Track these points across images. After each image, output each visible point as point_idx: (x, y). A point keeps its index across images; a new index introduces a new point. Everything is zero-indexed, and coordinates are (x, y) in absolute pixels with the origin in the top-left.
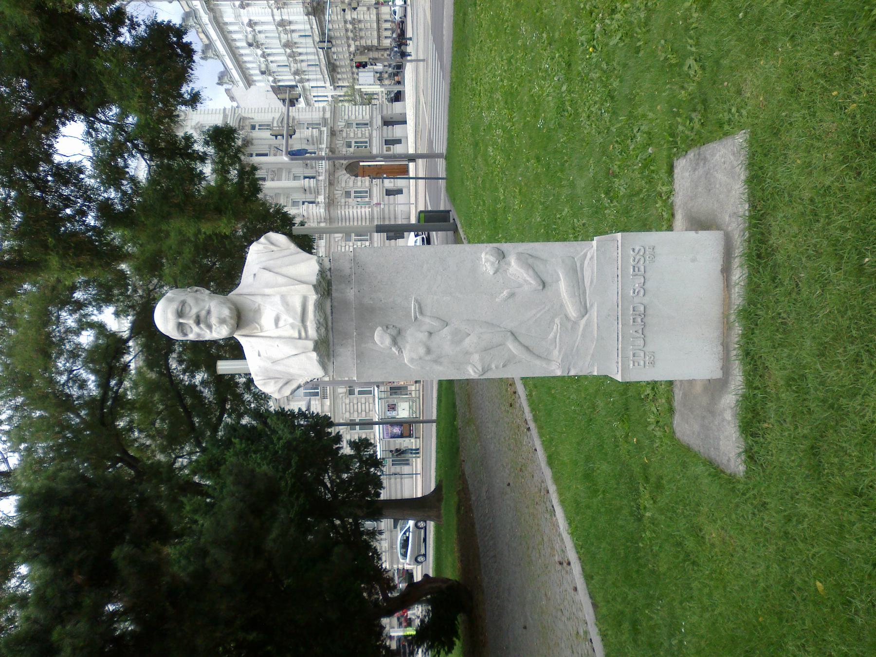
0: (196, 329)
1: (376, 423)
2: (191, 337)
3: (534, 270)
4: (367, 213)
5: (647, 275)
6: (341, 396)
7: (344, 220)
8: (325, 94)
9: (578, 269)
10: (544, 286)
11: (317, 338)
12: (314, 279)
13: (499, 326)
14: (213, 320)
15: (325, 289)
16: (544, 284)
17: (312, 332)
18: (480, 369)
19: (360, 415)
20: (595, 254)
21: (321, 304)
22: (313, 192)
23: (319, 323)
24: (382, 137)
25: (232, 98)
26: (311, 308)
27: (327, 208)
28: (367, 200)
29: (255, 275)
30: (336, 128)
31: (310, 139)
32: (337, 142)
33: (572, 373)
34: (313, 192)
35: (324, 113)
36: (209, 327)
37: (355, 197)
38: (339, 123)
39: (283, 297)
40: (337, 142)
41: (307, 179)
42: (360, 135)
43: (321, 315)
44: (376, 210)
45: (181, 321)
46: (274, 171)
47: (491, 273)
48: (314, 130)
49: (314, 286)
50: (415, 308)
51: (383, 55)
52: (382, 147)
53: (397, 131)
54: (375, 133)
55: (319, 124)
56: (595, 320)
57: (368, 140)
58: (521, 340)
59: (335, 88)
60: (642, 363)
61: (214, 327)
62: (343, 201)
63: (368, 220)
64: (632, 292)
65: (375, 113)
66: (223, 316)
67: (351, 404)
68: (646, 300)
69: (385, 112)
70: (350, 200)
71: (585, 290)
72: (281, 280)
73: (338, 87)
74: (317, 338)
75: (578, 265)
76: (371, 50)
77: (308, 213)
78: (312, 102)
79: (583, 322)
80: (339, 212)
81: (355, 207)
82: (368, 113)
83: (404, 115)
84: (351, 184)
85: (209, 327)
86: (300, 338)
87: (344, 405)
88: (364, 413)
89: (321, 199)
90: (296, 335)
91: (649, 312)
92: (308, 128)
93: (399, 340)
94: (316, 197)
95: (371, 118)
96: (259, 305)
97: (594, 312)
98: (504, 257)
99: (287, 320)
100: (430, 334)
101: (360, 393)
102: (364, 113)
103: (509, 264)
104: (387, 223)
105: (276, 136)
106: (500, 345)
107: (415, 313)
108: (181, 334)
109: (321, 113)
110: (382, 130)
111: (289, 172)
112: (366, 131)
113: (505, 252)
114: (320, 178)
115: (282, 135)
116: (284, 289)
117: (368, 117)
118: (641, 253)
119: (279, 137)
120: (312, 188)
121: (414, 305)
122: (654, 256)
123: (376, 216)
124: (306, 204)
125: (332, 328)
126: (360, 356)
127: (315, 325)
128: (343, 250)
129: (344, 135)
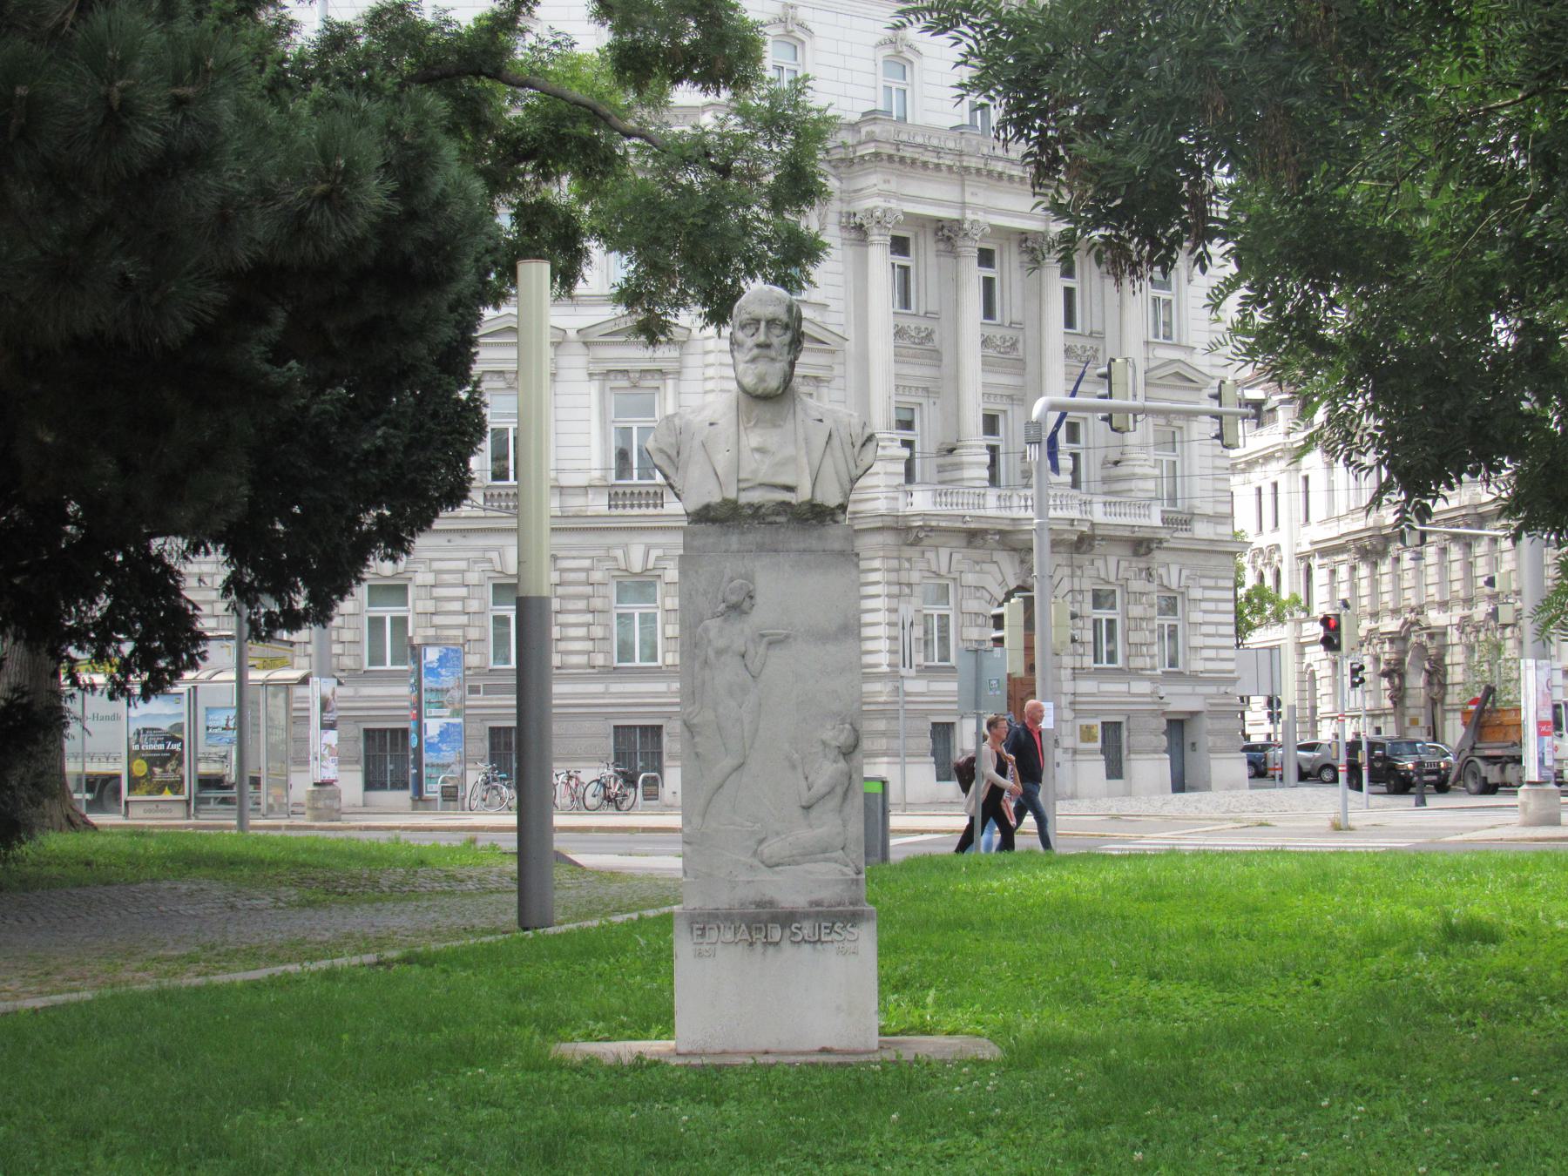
9: (827, 855)
12: (819, 500)
13: (751, 747)
17: (745, 498)
27: (889, 522)
28: (919, 659)
29: (821, 421)
30: (1159, 556)
32: (1112, 561)
38: (1174, 570)
39: (793, 460)
40: (1112, 561)
41: (987, 459)
45: (763, 324)
46: (1014, 346)
50: (777, 634)
51: (1414, 722)
53: (1151, 768)
54: (1142, 687)
57: (1120, 663)
59: (1304, 557)
61: (753, 367)
65: (1212, 690)
66: (768, 379)
72: (817, 455)
73: (1309, 569)
76: (1429, 683)
79: (756, 862)
80: (877, 564)
81: (894, 617)
82: (1210, 666)
83: (1204, 786)
84: (972, 605)
86: (739, 481)
89: (922, 501)
90: (742, 476)
92: (1158, 463)
95: (1195, 678)
96: (780, 426)
107: (772, 635)
109: (1208, 509)
115: (1110, 395)
116: (804, 460)
117: (1198, 665)
120: (956, 475)
124: (906, 453)
129: (1137, 585)
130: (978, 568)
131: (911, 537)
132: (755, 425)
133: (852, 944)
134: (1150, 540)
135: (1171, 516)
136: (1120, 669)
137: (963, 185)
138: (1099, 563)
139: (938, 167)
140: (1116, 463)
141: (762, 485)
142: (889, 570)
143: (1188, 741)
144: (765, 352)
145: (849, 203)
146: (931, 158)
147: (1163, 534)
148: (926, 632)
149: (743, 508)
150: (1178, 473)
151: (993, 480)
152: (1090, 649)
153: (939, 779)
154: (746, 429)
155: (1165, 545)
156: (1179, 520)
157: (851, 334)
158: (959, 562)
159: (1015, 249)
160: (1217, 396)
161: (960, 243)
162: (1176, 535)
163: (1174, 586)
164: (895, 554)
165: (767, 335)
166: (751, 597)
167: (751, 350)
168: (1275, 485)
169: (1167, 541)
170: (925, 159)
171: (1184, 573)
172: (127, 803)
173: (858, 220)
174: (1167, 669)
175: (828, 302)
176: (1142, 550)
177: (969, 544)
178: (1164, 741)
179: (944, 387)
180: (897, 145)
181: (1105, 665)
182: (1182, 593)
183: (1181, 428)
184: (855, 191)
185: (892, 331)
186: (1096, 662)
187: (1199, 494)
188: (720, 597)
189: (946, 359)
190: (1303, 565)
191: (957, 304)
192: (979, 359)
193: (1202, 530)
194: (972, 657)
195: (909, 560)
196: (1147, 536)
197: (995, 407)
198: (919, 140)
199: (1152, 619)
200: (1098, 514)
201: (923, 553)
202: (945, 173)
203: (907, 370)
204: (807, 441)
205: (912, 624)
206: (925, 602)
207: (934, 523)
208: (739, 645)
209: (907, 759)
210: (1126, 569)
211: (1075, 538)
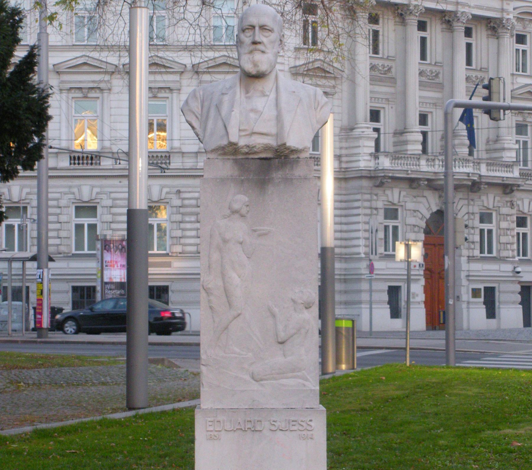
3: (295, 334)
4: (355, 250)
9: (295, 374)
10: (282, 343)
15: (282, 152)
20: (308, 389)
21: (268, 149)
22: (399, 148)
23: (253, 147)
24: (498, 282)
34: (399, 148)
37: (386, 228)
38: (526, 202)
42: (503, 239)
43: (259, 149)
44: (363, 266)
45: (257, 28)
46: (437, 75)
47: (293, 298)
48: (514, 154)
50: (263, 230)
52: (482, 281)
54: (508, 267)
57: (494, 254)
58: (233, 322)
60: (211, 428)
61: (251, 57)
62: (380, 204)
63: (344, 251)
64: (275, 419)
70: (381, 217)
75: (299, 374)
77: (359, 138)
79: (247, 377)
84: (411, 220)
86: (240, 130)
89: (385, 163)
92: (517, 142)
93: (237, 216)
94: (387, 154)
97: (255, 386)
98: (306, 308)
100: (241, 243)
107: (260, 230)
110: (513, 282)
111: (435, 105)
112: (510, 252)
113: (311, 309)
114: (423, 162)
118: (309, 428)
122: (304, 438)
123: (352, 265)
125: (247, 158)
126: (223, 181)
127: (251, 144)
129: (505, 210)
130: (415, 200)
131: (378, 183)
149: (242, 148)
152: (478, 246)
155: (521, 188)
158: (404, 196)
161: (407, 18)
162: (527, 182)
174: (521, 257)
176: (508, 191)
177: (411, 187)
178: (519, 298)
181: (486, 255)
186: (481, 253)
195: (376, 195)
196: (510, 183)
199: (513, 229)
201: (384, 191)
203: (377, 88)
205: (377, 231)
211: (470, 183)
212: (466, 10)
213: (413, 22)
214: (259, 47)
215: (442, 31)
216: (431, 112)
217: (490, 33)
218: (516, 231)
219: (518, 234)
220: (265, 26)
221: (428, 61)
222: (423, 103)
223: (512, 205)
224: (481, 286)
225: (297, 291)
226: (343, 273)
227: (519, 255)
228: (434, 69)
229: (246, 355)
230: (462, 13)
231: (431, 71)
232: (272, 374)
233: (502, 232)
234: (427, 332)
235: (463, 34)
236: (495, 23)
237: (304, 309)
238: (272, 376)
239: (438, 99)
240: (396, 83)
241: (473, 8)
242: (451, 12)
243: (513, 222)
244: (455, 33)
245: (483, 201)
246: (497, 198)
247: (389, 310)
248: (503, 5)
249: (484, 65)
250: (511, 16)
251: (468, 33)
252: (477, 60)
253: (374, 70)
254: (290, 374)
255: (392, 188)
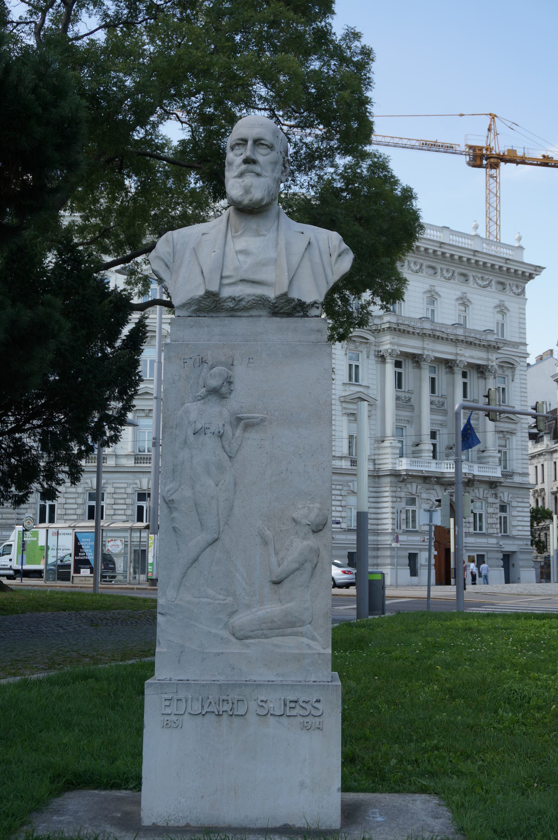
0: (239, 160)
1: (97, 524)
2: (230, 156)
5: (284, 720)
6: (138, 482)
7: (375, 495)
8: (546, 480)
9: (295, 629)
11: (221, 296)
12: (295, 295)
13: (226, 524)
14: (249, 179)
16: (277, 583)
17: (226, 292)
18: (173, 497)
19: (109, 507)
20: (314, 652)
23: (240, 300)
24: (487, 551)
25: (541, 359)
26: (259, 291)
28: (404, 527)
29: (303, 233)
30: (500, 489)
31: (485, 454)
33: (160, 618)
35: (521, 474)
36: (241, 175)
37: (407, 511)
38: (506, 494)
42: (490, 521)
43: (250, 304)
45: (250, 143)
46: (443, 404)
47: (295, 515)
49: (285, 294)
50: (253, 418)
53: (497, 574)
54: (493, 541)
55: (505, 467)
56: (228, 651)
57: (484, 531)
60: (168, 711)
61: (240, 180)
63: (375, 527)
64: (264, 698)
65: (521, 543)
66: (253, 190)
67: (125, 496)
68: (252, 718)
69: (520, 556)
70: (403, 504)
71: (268, 638)
74: (221, 296)
75: (300, 629)
78: (535, 461)
79: (226, 634)
83: (517, 580)
85: (241, 175)
86: (222, 277)
87: (125, 485)
88: (112, 512)
89: (404, 465)
90: (225, 274)
91: (236, 720)
95: (514, 538)
97: (235, 647)
98: (314, 532)
99: (247, 262)
101: (140, 509)
102: (521, 528)
103: (304, 538)
104: (370, 553)
105: (487, 396)
106: (202, 526)
107: (248, 418)
108: (234, 143)
109: (520, 471)
113: (321, 533)
115: (489, 404)
116: (284, 261)
117: (515, 533)
118: (314, 712)
119: (487, 400)
120: (420, 455)
121: (258, 417)
122: (306, 728)
123: (380, 538)
124: (400, 445)
127: (237, 295)
128: (334, 503)
129: (491, 500)
130: (428, 491)
131: (401, 479)
132: (242, 235)
133: (318, 720)
134: (496, 482)
135: (505, 473)
136: (484, 533)
137: (423, 343)
138: (476, 491)
139: (413, 333)
140: (483, 451)
141: (242, 281)
142: (392, 492)
143: (511, 563)
144: (252, 167)
145: (378, 346)
146: (411, 330)
147: (502, 480)
148: (407, 518)
149: (225, 301)
150: (508, 459)
151: (434, 457)
152: (472, 525)
153: (411, 576)
154: (232, 237)
155: (502, 484)
156: (507, 475)
157: (379, 398)
158: (420, 489)
159: (443, 367)
160: (535, 409)
161: (422, 363)
162: (507, 480)
163: (506, 501)
164: (395, 485)
165: (253, 151)
166: (230, 383)
167: (239, 166)
168: (543, 465)
169: (503, 483)
170: (409, 330)
171: (510, 496)
172: (73, 577)
173: (382, 353)
174: (503, 534)
175: (370, 385)
176: (493, 486)
177: (424, 482)
178: (502, 563)
179: (416, 421)
180: (398, 324)
181: (478, 531)
182: (509, 504)
183: (509, 438)
184: (381, 342)
185: (395, 398)
186: (474, 530)
187: (515, 465)
188: (201, 383)
189: (416, 409)
190: (553, 497)
191: (420, 387)
192: (429, 409)
193: (517, 479)
194: (428, 513)
195: (400, 488)
196: (495, 480)
197: (435, 428)
198: (406, 323)
199: (497, 514)
200: (476, 473)
201: (406, 485)
202: (416, 336)
203: (400, 413)
204: (288, 245)
205: (401, 511)
206: (407, 505)
207: (410, 473)
208: (216, 425)
209: (398, 567)
210: (487, 494)
211: (467, 480)
212: (463, 359)
213: (425, 366)
214: (257, 169)
215: (446, 374)
216: (439, 430)
217: (479, 375)
218: (498, 516)
219: (500, 517)
220: (262, 139)
221: (437, 394)
222: (433, 423)
223: (496, 497)
224: (475, 554)
225: (300, 506)
226: (375, 543)
227: (501, 532)
228: (441, 399)
229: (224, 600)
230: (460, 361)
231: (439, 401)
232: (262, 630)
233: (489, 515)
234: (437, 587)
235: (461, 376)
236: (483, 368)
237: (312, 533)
238: (262, 632)
239: (443, 421)
240: (414, 409)
241: (468, 357)
242: (452, 360)
243: (497, 508)
244: (455, 375)
245: (476, 493)
246: (486, 491)
247: (409, 570)
248: (488, 356)
249: (476, 398)
250: (494, 364)
251: (464, 375)
252: (470, 394)
253: (399, 400)
254: (290, 630)
255: (411, 483)
